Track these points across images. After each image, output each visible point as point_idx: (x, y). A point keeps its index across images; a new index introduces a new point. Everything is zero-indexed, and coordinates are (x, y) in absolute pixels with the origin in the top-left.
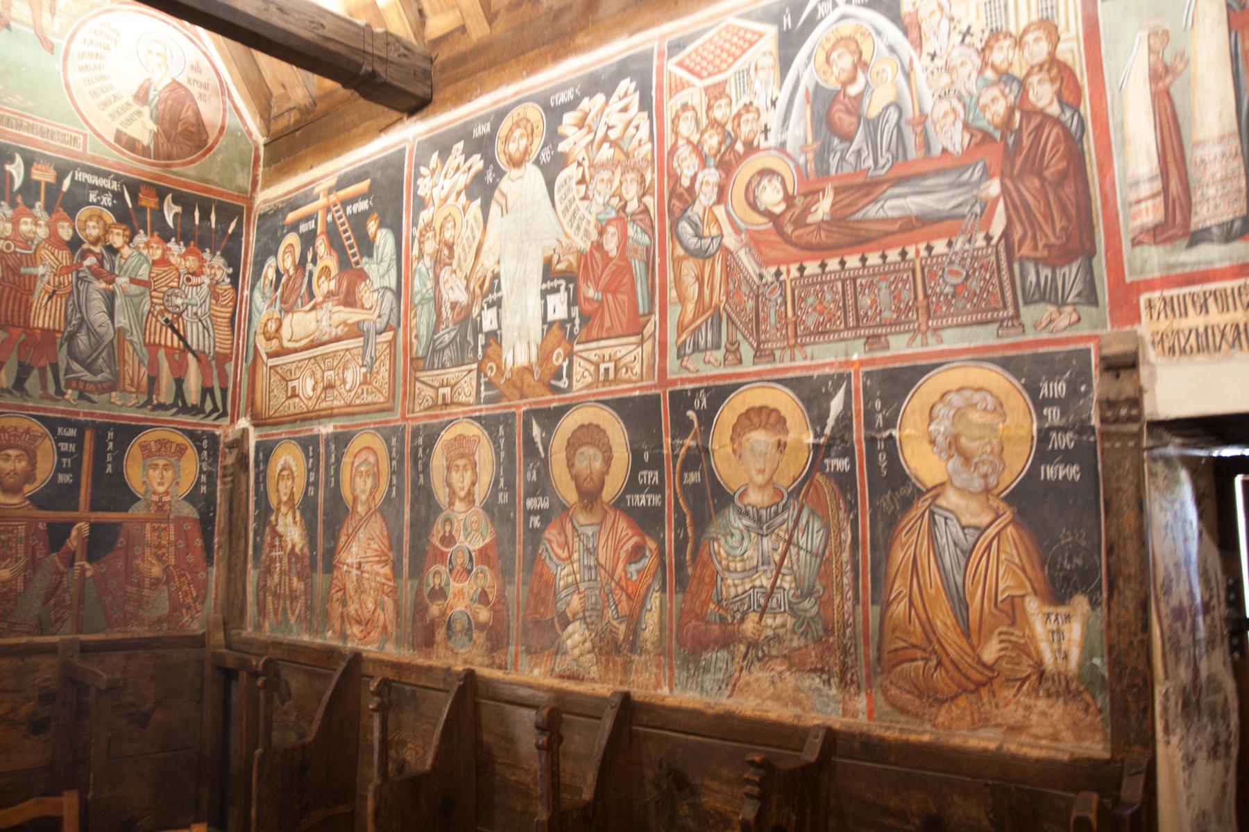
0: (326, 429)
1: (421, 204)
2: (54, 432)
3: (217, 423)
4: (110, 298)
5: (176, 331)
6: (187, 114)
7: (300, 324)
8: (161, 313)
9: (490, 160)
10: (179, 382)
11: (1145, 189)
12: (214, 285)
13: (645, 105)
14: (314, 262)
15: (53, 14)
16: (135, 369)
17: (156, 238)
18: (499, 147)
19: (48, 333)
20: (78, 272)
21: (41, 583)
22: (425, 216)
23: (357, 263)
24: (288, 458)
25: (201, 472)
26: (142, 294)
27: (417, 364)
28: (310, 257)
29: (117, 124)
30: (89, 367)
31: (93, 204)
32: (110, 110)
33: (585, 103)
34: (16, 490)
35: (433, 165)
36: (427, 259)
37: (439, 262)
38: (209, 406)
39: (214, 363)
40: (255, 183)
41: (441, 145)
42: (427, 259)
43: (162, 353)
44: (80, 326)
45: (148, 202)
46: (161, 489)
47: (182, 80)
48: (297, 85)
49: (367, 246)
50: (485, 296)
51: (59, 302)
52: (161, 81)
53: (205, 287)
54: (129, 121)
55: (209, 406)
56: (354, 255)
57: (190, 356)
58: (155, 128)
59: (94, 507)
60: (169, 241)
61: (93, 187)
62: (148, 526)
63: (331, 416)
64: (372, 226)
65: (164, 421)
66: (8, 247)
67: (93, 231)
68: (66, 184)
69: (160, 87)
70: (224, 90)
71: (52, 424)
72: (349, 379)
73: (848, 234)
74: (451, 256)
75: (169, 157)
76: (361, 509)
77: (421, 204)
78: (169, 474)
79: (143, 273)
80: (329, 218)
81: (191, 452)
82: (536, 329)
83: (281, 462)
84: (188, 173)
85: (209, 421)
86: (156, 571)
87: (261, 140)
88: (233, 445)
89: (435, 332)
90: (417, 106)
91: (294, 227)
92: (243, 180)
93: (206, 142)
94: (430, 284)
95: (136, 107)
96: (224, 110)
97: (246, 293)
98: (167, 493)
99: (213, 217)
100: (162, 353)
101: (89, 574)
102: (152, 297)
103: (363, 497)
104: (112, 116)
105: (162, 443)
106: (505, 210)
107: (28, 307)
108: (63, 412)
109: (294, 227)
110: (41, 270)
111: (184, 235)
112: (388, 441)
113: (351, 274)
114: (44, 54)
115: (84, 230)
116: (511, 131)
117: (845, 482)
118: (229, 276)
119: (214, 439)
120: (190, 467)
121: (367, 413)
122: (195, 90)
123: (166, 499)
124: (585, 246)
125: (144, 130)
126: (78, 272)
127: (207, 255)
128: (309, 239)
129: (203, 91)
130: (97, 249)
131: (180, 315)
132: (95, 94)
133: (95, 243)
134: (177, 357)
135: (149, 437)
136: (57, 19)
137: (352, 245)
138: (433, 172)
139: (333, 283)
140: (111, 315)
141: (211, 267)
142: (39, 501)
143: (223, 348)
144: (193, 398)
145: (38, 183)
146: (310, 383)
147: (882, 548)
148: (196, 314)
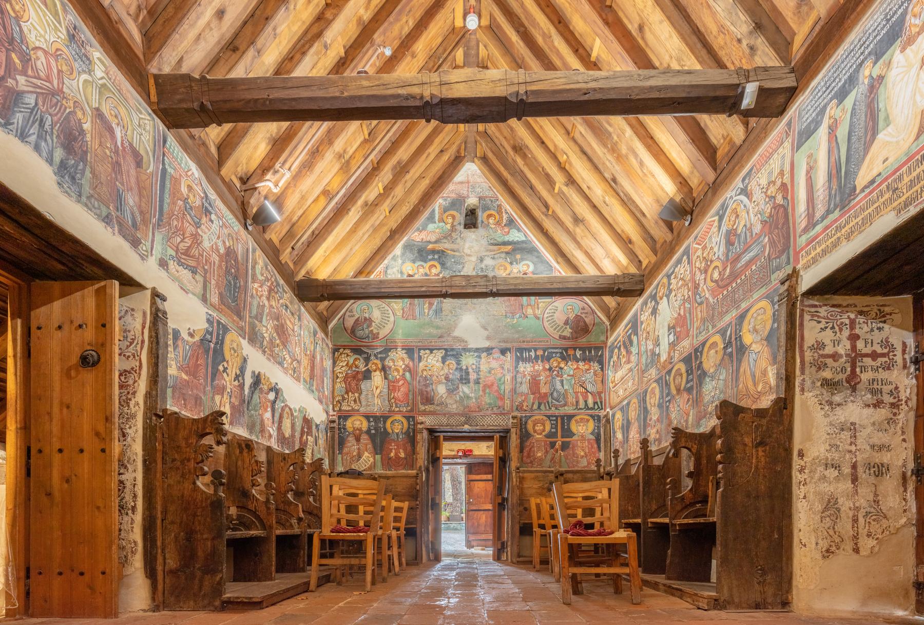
0: (625, 402)
4: (562, 382)
7: (620, 374)
10: (586, 402)
11: (803, 216)
12: (595, 372)
13: (689, 263)
16: (571, 399)
19: (546, 394)
21: (549, 457)
24: (619, 415)
27: (643, 372)
33: (677, 270)
34: (541, 434)
49: (631, 342)
51: (547, 385)
52: (572, 316)
59: (562, 437)
67: (555, 364)
70: (593, 312)
71: (548, 417)
73: (734, 276)
77: (642, 323)
79: (571, 373)
81: (591, 421)
82: (667, 346)
88: (606, 416)
90: (640, 293)
92: (603, 338)
105: (582, 419)
111: (584, 360)
113: (629, 352)
117: (731, 355)
119: (599, 417)
120: (591, 425)
122: (583, 316)
124: (676, 316)
125: (568, 332)
135: (578, 417)
142: (547, 436)
143: (601, 389)
147: (738, 370)
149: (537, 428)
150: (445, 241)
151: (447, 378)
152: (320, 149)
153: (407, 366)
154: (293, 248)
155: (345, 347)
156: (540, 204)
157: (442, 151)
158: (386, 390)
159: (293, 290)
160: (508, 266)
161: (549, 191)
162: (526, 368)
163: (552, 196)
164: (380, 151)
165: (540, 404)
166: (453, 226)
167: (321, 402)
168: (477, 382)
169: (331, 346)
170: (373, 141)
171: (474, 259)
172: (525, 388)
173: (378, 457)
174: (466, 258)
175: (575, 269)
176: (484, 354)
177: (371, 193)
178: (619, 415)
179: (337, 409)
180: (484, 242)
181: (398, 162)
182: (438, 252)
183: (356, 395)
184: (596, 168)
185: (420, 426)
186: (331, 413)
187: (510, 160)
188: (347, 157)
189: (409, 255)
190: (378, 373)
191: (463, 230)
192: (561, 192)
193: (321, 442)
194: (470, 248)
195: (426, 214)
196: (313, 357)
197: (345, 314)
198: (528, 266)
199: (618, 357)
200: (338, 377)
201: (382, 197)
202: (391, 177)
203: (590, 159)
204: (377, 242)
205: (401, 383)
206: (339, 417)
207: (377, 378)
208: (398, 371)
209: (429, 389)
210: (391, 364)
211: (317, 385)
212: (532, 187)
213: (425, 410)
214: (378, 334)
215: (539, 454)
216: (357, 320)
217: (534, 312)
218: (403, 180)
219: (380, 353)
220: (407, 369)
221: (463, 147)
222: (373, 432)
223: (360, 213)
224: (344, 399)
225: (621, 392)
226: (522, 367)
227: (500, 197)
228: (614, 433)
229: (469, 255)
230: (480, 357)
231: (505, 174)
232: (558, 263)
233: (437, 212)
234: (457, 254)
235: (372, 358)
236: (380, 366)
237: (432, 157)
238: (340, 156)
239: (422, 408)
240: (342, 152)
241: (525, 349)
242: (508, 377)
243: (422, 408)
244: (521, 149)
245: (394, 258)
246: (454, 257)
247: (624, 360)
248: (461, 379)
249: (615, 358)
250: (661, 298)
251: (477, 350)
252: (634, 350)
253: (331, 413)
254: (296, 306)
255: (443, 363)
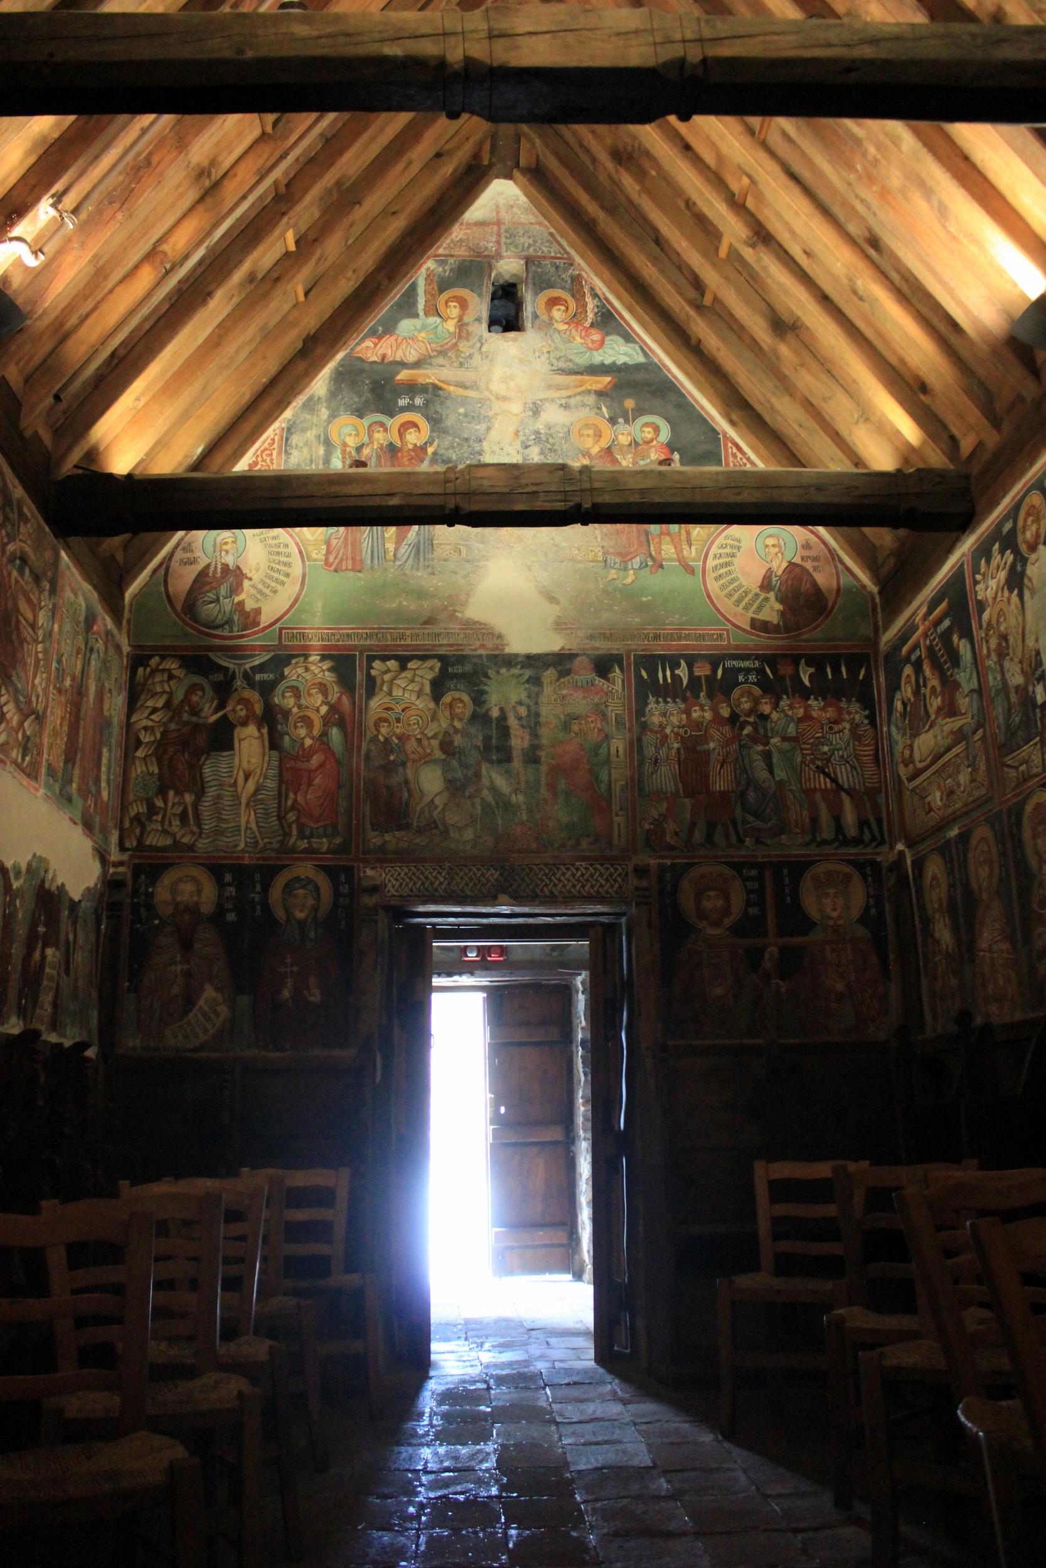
0: (954, 832)
1: (981, 606)
2: (741, 875)
3: (878, 850)
4: (767, 756)
5: (827, 775)
6: (806, 587)
7: (926, 742)
8: (812, 761)
9: (1016, 552)
10: (838, 819)
12: (855, 727)
14: (925, 686)
15: (690, 545)
17: (797, 699)
18: (1020, 538)
19: (724, 794)
20: (740, 741)
22: (986, 616)
23: (951, 675)
24: (935, 868)
25: (869, 896)
26: (794, 748)
28: (921, 681)
29: (750, 614)
30: (757, 815)
31: (742, 683)
32: (743, 604)
34: (716, 924)
35: (982, 570)
36: (993, 655)
37: (1002, 654)
38: (867, 837)
39: (866, 797)
40: (876, 629)
41: (983, 551)
42: (993, 655)
43: (818, 796)
44: (748, 785)
45: (786, 670)
46: (835, 914)
47: (797, 560)
48: (883, 537)
49: (955, 658)
50: (1034, 674)
52: (779, 566)
53: (846, 731)
54: (760, 609)
55: (867, 837)
56: (948, 669)
57: (843, 795)
58: (781, 607)
60: (808, 699)
61: (740, 670)
62: (828, 948)
63: (954, 820)
64: (955, 638)
65: (827, 855)
66: (686, 732)
67: (746, 706)
68: (720, 672)
69: (780, 573)
71: (737, 867)
72: (962, 782)
74: (1008, 647)
75: (798, 629)
76: (985, 895)
77: (981, 606)
78: (840, 901)
79: (791, 730)
80: (928, 642)
81: (857, 879)
83: (930, 873)
84: (814, 636)
85: (869, 850)
86: (840, 986)
87: (874, 589)
89: (1009, 718)
90: (965, 522)
91: (907, 660)
92: (865, 630)
93: (826, 606)
94: (999, 677)
95: (763, 595)
96: (838, 574)
97: (885, 729)
98: (840, 917)
99: (844, 670)
100: (818, 796)
101: (783, 990)
102: (802, 750)
103: (985, 884)
104: (746, 608)
106: (1033, 593)
107: (707, 777)
108: (744, 856)
109: (907, 660)
110: (712, 745)
112: (992, 826)
113: (950, 685)
114: (688, 577)
115: (739, 706)
116: (1025, 520)
118: (867, 717)
120: (858, 894)
121: (977, 807)
122: (808, 565)
123: (840, 922)
125: (772, 611)
126: (740, 741)
127: (843, 704)
128: (918, 666)
129: (816, 564)
130: (751, 720)
131: (828, 760)
132: (729, 595)
133: (748, 715)
134: (831, 797)
135: (820, 869)
136: (693, 548)
137: (944, 659)
138: (984, 575)
139: (939, 699)
140: (771, 771)
141: (849, 713)
142: (736, 930)
144: (852, 831)
145: (699, 677)
146: (938, 794)
148: (842, 756)
149: (707, 904)
150: (441, 360)
151: (446, 746)
152: (155, 160)
153: (334, 708)
154: (57, 398)
155: (164, 653)
156: (683, 282)
157: (438, 155)
158: (271, 784)
159: (43, 507)
160: (605, 426)
161: (704, 254)
162: (666, 715)
163: (713, 265)
164: (297, 160)
165: (711, 827)
166: (461, 325)
167: (88, 826)
168: (532, 758)
169: (126, 649)
170: (284, 137)
171: (516, 407)
172: (665, 777)
173: (244, 1001)
174: (497, 406)
175: (794, 459)
176: (549, 675)
177: (264, 257)
178: (935, 868)
179: (131, 843)
180: (541, 366)
181: (338, 183)
182: (424, 389)
183: (189, 798)
184: (826, 212)
185: (370, 901)
186: (115, 855)
187: (602, 178)
188: (216, 174)
189: (349, 397)
190: (251, 730)
191: (486, 334)
192: (735, 256)
193: (80, 957)
194: (505, 380)
195: (396, 295)
196: (80, 691)
197: (171, 555)
198: (657, 430)
199: (917, 692)
200: (139, 743)
201: (290, 261)
202: (317, 215)
203: (808, 192)
204: (271, 366)
205: (316, 760)
206: (137, 870)
207: (250, 743)
208: (307, 722)
209: (396, 779)
210: (290, 702)
211: (83, 777)
212: (659, 240)
213: (382, 848)
214: (258, 612)
215: (718, 991)
216: (203, 573)
217: (679, 551)
218: (346, 222)
219: (261, 668)
220: (335, 717)
221: (487, 146)
222: (231, 917)
223: (236, 300)
224: (152, 810)
225: (936, 798)
226: (655, 711)
227: (578, 259)
228: (927, 921)
229: (505, 399)
230: (536, 681)
231: (592, 208)
232: (732, 423)
233: (421, 290)
234: (472, 394)
235: (239, 683)
236: (258, 708)
237: (415, 168)
238: (202, 173)
239: (375, 839)
240: (206, 163)
241: (663, 659)
242: (618, 744)
243: (375, 839)
244: (630, 157)
245: (310, 406)
246: (464, 401)
247: (937, 702)
248: (487, 747)
249: (907, 691)
250: (1033, 548)
251: (531, 660)
252: (966, 679)
253: (115, 855)
254: (48, 554)
255: (437, 696)
